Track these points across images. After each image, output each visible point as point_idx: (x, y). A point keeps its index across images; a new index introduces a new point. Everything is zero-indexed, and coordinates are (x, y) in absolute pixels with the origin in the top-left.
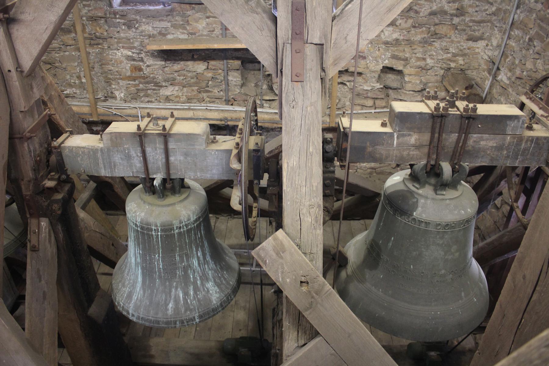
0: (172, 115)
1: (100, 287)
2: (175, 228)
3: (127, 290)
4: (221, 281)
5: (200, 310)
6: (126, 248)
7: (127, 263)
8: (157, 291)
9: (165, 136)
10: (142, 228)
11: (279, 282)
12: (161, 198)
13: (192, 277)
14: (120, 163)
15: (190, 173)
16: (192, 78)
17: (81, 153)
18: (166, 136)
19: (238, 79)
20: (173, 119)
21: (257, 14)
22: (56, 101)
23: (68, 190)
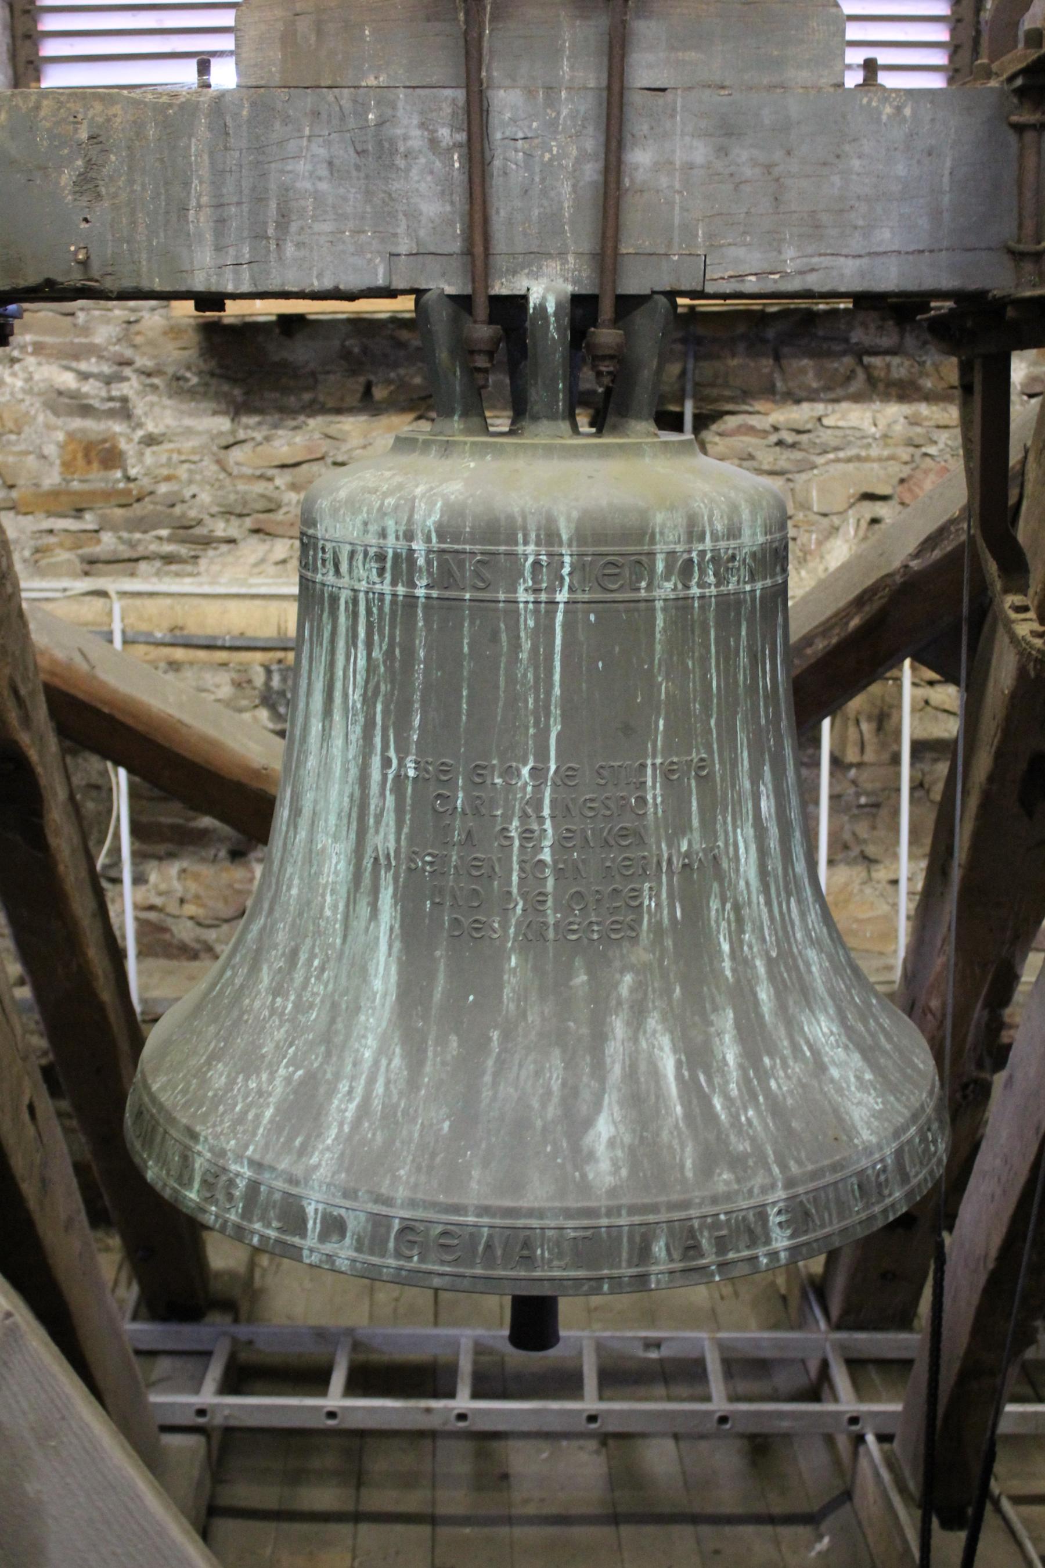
2: (660, 566)
5: (794, 1168)
8: (507, 1036)
13: (726, 947)
14: (318, 198)
15: (741, 252)
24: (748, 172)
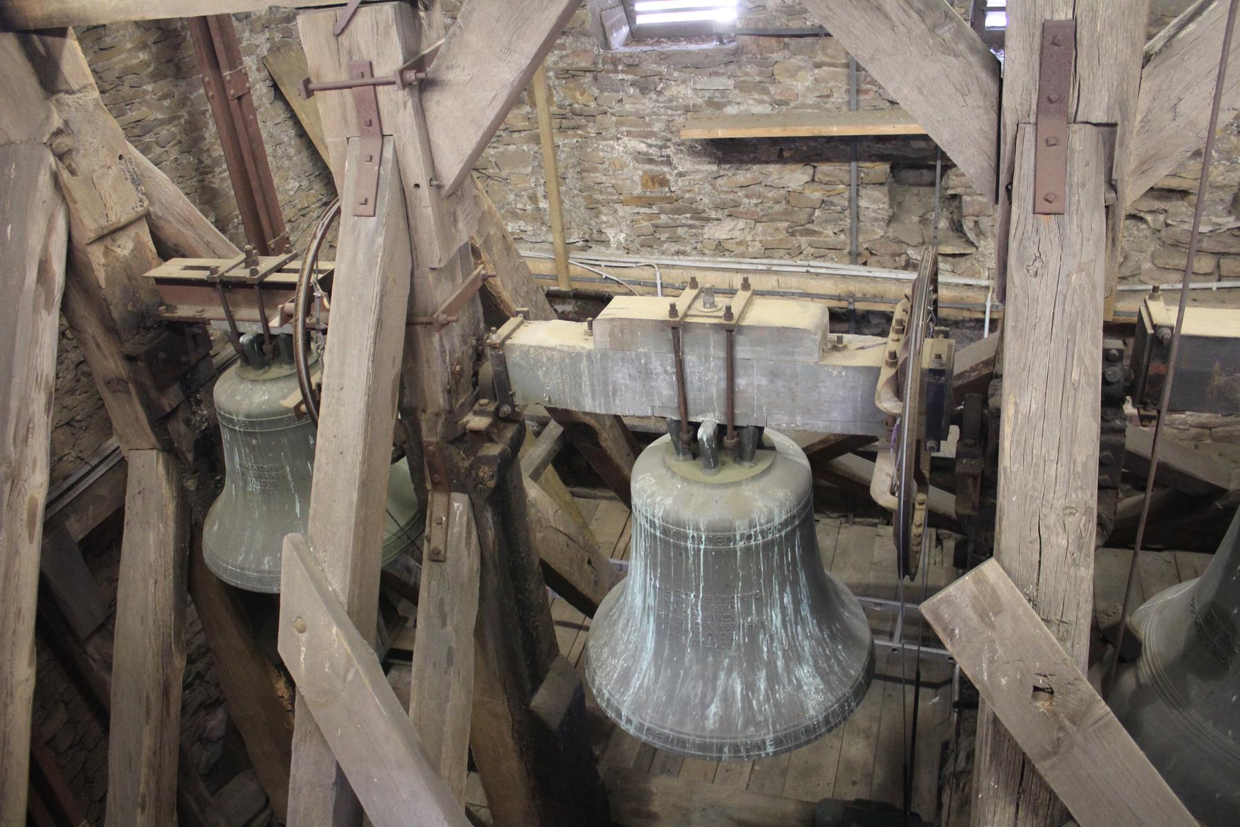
0: (746, 285)
1: (558, 651)
2: (738, 538)
3: (620, 664)
4: (829, 666)
5: (778, 727)
6: (620, 573)
7: (623, 605)
8: (685, 673)
9: (730, 331)
10: (665, 531)
11: (982, 682)
12: (710, 468)
13: (765, 649)
15: (780, 416)
16: (777, 202)
17: (545, 360)
18: (731, 331)
19: (881, 206)
20: (748, 294)
21: (956, 56)
22: (497, 248)
23: (512, 438)
24: (782, 390)
